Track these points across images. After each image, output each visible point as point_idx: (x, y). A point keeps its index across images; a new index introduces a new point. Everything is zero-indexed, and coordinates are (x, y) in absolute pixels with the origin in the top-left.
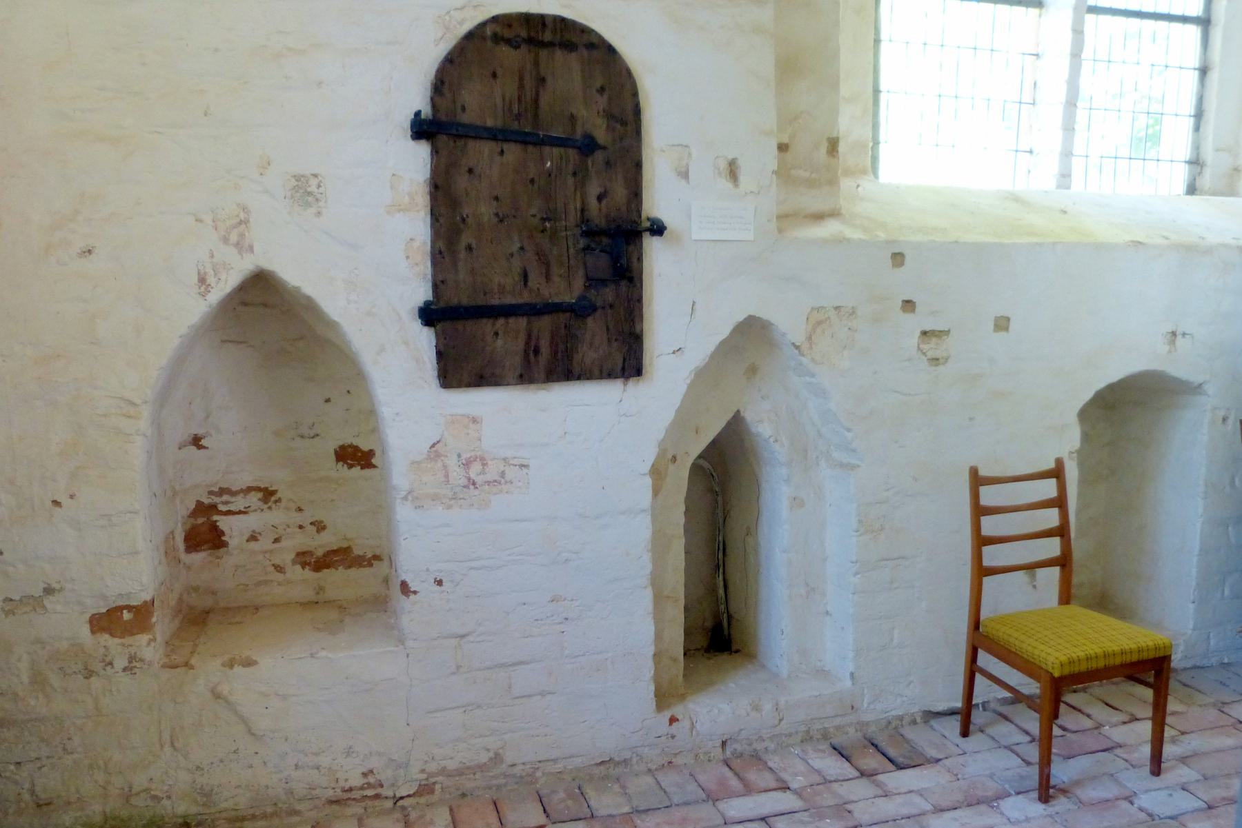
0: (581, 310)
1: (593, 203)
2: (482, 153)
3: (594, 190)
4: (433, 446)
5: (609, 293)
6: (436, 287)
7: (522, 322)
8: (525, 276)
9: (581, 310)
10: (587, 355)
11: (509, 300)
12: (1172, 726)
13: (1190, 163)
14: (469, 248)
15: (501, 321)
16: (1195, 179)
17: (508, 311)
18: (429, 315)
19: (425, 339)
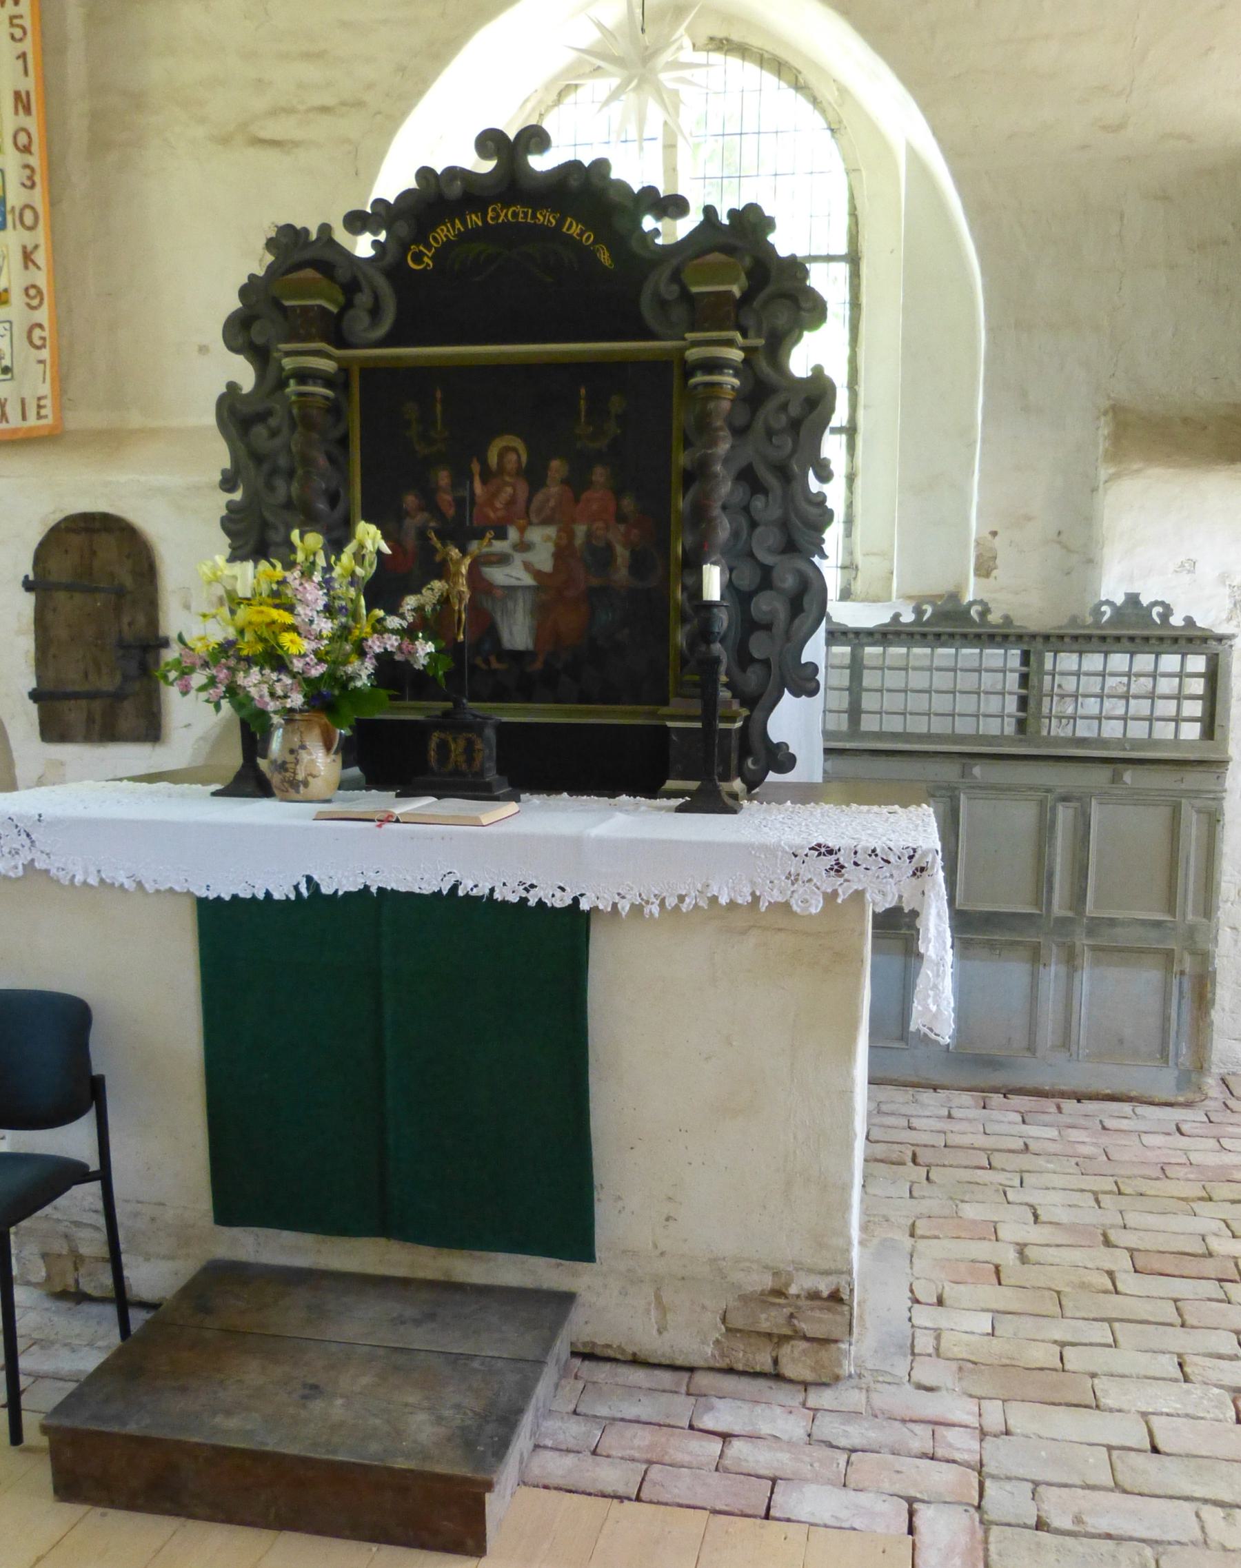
0: (118, 697)
1: (125, 627)
2: (61, 596)
3: (126, 620)
4: (40, 778)
5: (137, 686)
6: (39, 678)
7: (83, 703)
8: (86, 675)
9: (118, 697)
10: (124, 725)
11: (77, 688)
12: (1044, 1314)
13: (843, 568)
14: (54, 656)
15: (73, 702)
16: (850, 584)
17: (76, 696)
18: (35, 696)
19: (33, 708)
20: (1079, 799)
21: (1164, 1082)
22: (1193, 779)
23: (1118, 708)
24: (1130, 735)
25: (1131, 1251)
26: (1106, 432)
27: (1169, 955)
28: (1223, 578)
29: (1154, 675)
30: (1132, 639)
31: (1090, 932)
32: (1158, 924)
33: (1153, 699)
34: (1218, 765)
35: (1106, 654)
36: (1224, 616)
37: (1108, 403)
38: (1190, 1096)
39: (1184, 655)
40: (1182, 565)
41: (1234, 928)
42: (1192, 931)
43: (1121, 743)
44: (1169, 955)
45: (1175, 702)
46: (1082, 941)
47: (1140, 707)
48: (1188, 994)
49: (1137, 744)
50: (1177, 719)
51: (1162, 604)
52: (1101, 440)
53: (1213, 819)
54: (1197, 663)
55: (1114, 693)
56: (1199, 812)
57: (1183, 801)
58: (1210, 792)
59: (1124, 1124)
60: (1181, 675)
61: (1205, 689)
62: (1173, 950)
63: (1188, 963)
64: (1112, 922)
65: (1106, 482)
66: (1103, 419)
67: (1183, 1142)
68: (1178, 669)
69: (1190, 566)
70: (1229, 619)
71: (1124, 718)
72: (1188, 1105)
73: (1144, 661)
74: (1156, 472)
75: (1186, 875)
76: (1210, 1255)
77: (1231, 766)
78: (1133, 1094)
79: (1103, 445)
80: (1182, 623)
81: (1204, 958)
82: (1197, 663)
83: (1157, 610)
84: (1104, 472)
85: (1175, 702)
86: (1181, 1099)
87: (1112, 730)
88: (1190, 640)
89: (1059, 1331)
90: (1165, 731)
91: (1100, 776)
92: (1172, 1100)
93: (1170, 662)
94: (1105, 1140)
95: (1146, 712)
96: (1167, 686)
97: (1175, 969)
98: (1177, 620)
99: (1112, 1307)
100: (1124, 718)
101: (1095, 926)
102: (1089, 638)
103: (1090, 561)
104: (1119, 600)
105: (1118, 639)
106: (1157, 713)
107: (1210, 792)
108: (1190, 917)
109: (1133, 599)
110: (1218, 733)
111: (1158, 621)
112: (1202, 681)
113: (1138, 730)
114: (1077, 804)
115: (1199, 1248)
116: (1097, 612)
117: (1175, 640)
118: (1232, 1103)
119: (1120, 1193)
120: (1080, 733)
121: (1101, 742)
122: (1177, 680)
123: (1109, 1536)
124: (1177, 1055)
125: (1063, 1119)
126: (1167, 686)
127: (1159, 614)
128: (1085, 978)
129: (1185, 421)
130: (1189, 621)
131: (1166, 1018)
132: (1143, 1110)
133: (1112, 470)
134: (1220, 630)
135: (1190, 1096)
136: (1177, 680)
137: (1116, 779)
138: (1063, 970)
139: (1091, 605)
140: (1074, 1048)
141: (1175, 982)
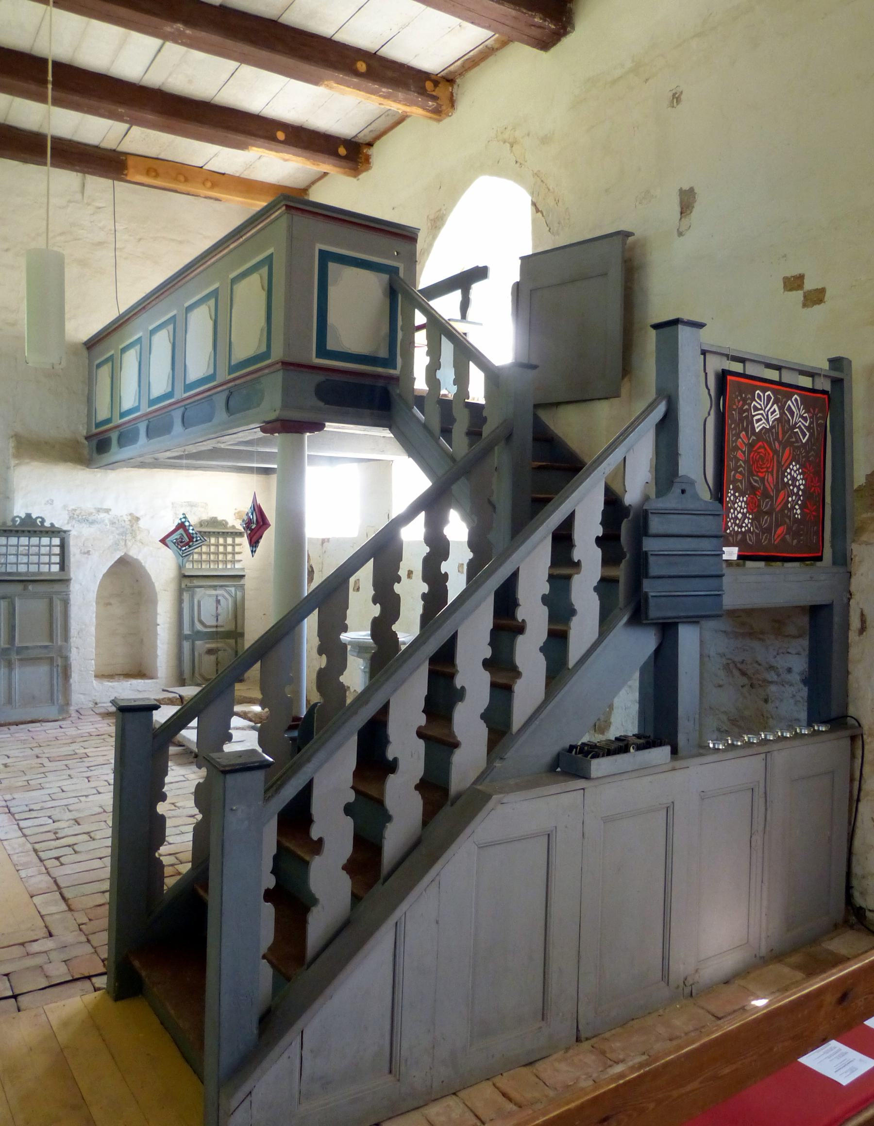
20: (9, 598)
21: (52, 711)
22: (57, 587)
23: (24, 559)
24: (30, 570)
25: (48, 758)
26: (13, 445)
27: (51, 659)
28: (65, 507)
29: (39, 546)
30: (29, 531)
31: (18, 653)
32: (46, 647)
33: (39, 555)
34: (66, 581)
35: (19, 537)
36: (66, 522)
37: (13, 434)
38: (64, 716)
39: (51, 538)
40: (48, 502)
41: (77, 648)
42: (60, 649)
43: (27, 573)
44: (51, 659)
45: (48, 557)
46: (14, 657)
47: (34, 559)
48: (61, 675)
49: (34, 574)
50: (49, 564)
51: (41, 518)
52: (11, 449)
53: (66, 603)
54: (56, 541)
55: (22, 553)
56: (60, 600)
57: (54, 596)
58: (64, 592)
59: (38, 729)
60: (50, 546)
61: (60, 551)
62: (53, 657)
63: (60, 661)
64: (27, 648)
65: (14, 466)
66: (11, 440)
67: (63, 730)
68: (49, 544)
69: (51, 502)
70: (68, 523)
71: (28, 564)
72: (64, 719)
73: (35, 540)
74: (35, 464)
75: (57, 627)
76: (77, 754)
77: (72, 581)
78: (40, 719)
79: (11, 451)
80: (49, 526)
81: (66, 659)
82: (56, 541)
83: (39, 520)
84: (13, 462)
85: (48, 557)
86: (61, 718)
87: (22, 569)
88: (53, 532)
89: (26, 778)
90: (45, 569)
91: (19, 587)
92: (56, 718)
93: (45, 541)
94: (31, 734)
95: (37, 561)
96: (44, 550)
97: (55, 664)
98: (47, 524)
99: (43, 770)
100: (28, 564)
101: (20, 650)
102: (11, 531)
103: (8, 498)
104: (23, 516)
105: (23, 531)
106: (52, 553)
107: (64, 592)
108: (59, 643)
109: (29, 516)
110: (66, 568)
111: (40, 524)
112: (59, 548)
113: (33, 568)
114: (10, 600)
115: (73, 753)
116: (13, 520)
117: (47, 532)
118: (81, 717)
119: (40, 746)
120: (9, 570)
121: (18, 574)
122: (48, 548)
123: (52, 807)
124: (58, 701)
125: (10, 732)
126: (44, 550)
127: (40, 522)
128: (17, 673)
129: (46, 443)
130: (52, 525)
131: (52, 685)
132: (44, 724)
133: (17, 462)
134: (65, 528)
135: (64, 716)
136: (48, 548)
137: (25, 589)
138: (6, 670)
139: (10, 518)
140: (13, 704)
141: (55, 670)
